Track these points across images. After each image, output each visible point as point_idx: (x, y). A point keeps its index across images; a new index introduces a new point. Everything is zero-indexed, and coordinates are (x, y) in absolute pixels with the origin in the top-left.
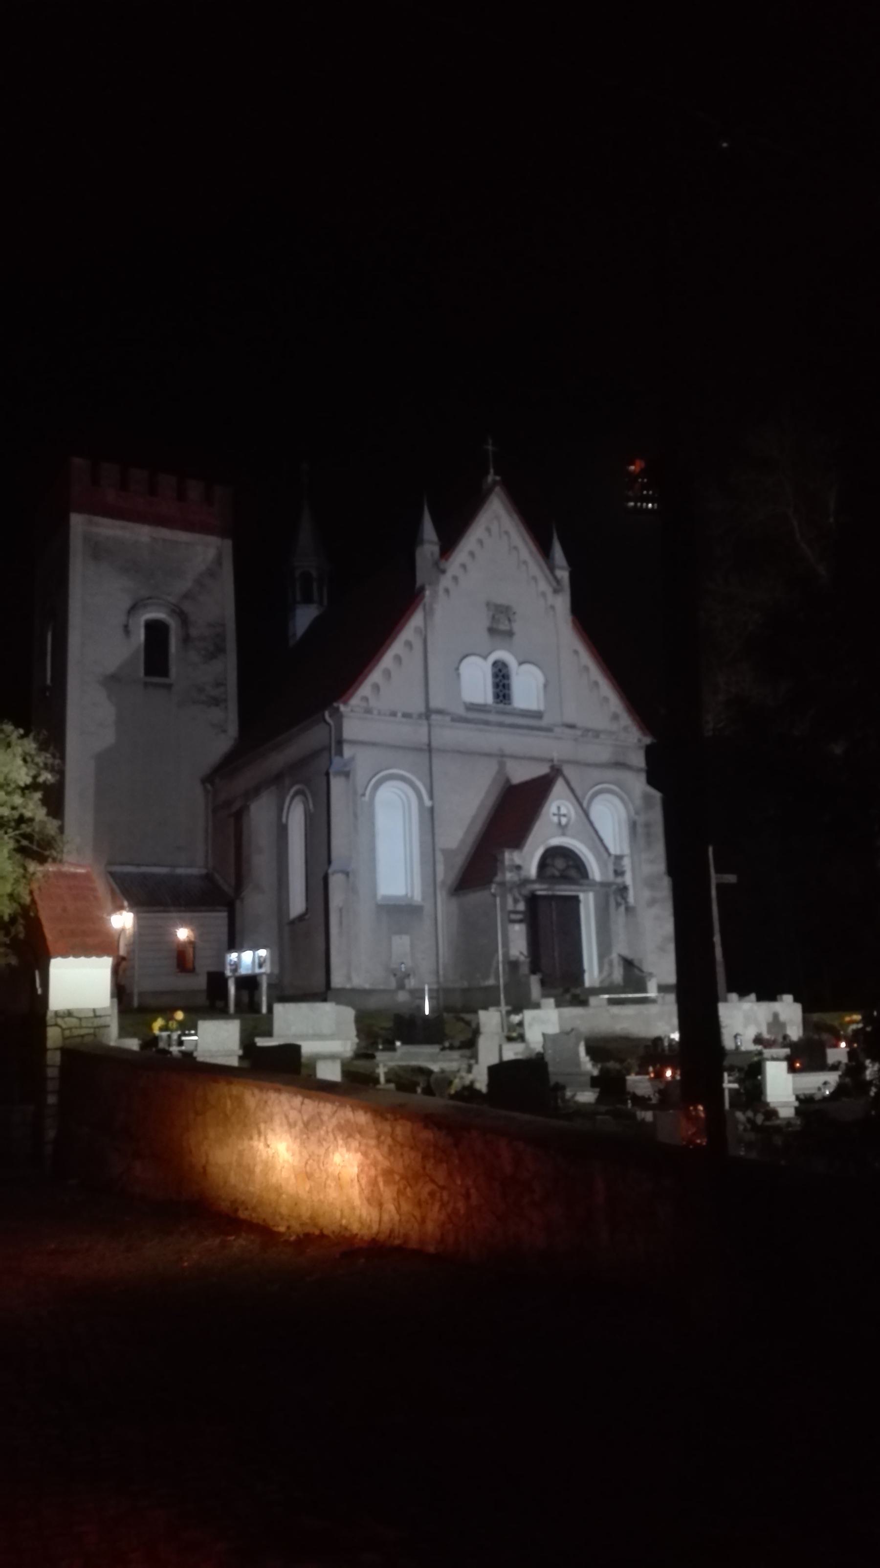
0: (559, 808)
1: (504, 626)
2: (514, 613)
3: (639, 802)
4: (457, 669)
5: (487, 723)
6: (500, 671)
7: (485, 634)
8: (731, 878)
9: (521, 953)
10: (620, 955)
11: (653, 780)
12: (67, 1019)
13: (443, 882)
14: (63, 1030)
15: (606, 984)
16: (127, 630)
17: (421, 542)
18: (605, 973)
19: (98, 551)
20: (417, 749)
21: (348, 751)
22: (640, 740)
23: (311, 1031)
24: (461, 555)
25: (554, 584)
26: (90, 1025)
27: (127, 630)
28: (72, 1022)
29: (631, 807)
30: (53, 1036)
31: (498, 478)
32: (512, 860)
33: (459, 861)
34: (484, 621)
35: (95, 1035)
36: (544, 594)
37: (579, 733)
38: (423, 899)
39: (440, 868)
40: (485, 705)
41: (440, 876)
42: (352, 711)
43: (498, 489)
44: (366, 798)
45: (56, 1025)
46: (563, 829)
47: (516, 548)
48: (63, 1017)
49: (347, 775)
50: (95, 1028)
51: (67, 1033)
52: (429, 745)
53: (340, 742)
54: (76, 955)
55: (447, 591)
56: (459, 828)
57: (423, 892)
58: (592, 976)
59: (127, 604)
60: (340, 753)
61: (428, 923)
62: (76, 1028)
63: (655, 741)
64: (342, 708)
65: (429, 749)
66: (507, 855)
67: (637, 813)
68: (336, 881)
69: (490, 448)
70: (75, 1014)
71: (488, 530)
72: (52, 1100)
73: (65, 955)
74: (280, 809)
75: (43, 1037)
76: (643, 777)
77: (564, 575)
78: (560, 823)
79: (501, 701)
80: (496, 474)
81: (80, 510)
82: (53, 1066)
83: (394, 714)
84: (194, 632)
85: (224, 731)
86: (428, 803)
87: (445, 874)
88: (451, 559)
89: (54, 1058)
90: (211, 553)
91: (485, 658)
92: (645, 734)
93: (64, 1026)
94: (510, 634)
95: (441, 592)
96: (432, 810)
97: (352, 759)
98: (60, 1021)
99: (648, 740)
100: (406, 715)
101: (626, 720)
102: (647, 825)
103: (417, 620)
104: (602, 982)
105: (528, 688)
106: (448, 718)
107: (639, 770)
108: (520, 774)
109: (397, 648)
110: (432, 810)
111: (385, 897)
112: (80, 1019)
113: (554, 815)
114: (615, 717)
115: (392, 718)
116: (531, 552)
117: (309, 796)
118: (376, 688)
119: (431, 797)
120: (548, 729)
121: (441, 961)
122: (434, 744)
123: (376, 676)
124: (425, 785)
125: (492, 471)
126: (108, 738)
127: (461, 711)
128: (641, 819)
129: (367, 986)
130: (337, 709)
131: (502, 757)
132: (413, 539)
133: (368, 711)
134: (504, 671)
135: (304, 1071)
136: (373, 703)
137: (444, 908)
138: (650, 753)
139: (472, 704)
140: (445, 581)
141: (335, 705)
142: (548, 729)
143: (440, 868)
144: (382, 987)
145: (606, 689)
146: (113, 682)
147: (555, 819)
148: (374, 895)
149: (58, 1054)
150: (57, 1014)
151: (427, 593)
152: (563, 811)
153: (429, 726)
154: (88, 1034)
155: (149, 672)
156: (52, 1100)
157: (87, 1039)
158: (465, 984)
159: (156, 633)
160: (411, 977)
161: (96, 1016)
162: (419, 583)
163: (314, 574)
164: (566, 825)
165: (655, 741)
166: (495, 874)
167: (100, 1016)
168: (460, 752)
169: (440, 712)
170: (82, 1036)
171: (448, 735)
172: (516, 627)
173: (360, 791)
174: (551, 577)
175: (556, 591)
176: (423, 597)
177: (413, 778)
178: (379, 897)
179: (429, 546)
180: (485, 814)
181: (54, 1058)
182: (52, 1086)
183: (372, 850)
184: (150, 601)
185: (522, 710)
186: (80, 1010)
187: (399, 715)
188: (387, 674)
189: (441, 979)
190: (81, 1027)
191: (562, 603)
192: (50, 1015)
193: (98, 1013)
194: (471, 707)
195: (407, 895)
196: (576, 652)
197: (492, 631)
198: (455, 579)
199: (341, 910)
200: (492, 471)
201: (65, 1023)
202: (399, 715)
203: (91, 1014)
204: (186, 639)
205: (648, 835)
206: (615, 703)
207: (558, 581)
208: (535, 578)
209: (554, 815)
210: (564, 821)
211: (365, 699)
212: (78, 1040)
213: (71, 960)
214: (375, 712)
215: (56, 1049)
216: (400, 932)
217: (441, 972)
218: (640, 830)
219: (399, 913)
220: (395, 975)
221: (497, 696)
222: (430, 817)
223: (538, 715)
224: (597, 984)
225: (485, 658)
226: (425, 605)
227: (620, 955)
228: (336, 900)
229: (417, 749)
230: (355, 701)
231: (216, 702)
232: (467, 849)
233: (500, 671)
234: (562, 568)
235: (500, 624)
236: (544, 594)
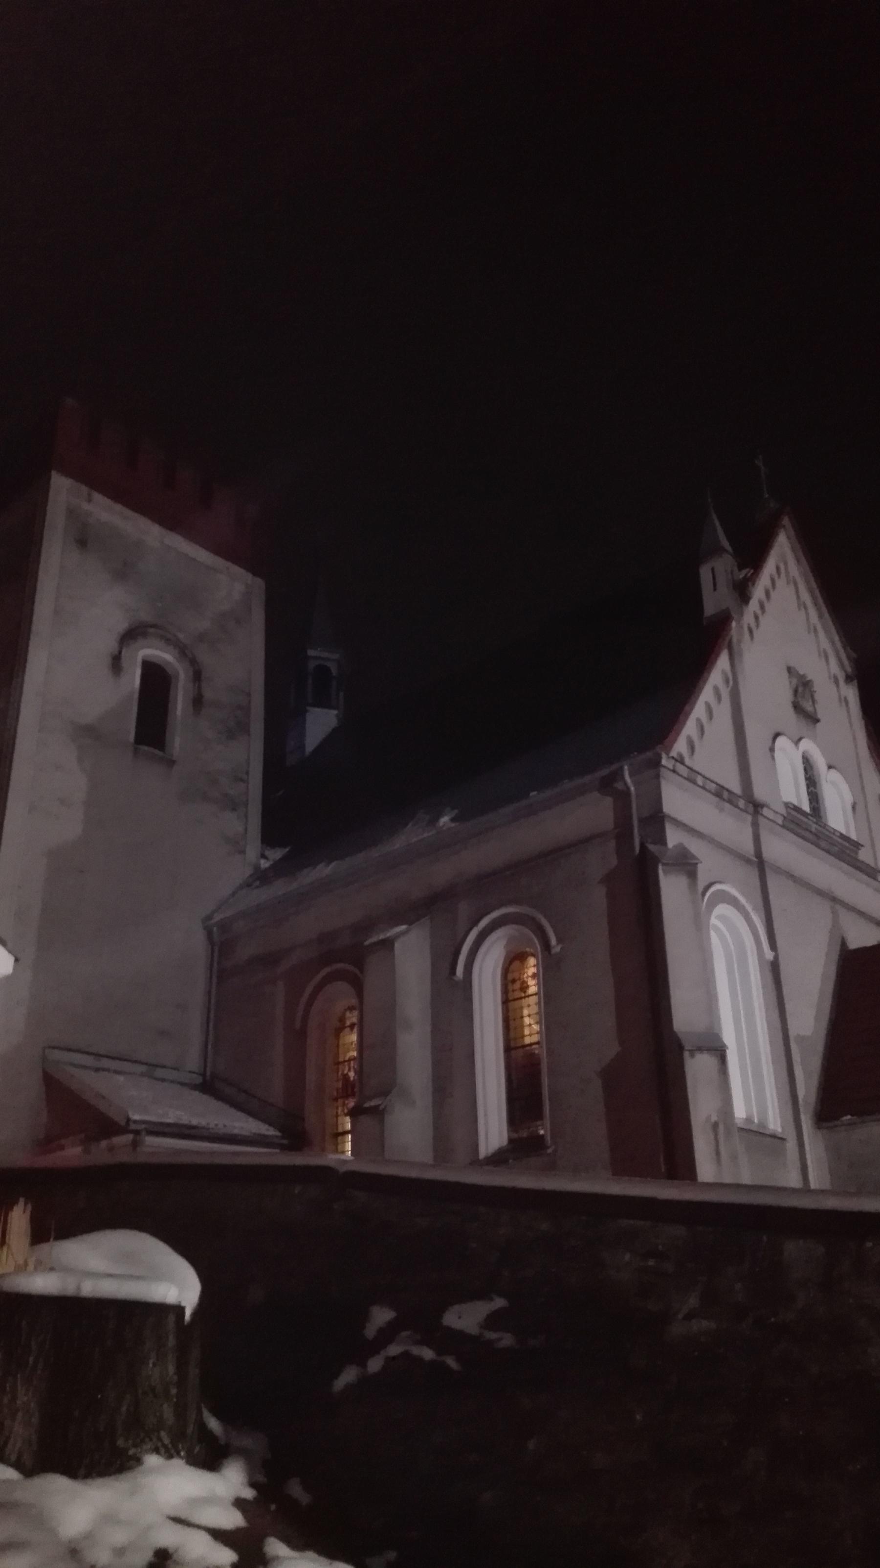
4: (772, 750)
16: (116, 663)
19: (83, 538)
27: (116, 663)
41: (801, 1093)
52: (758, 854)
59: (122, 626)
65: (760, 864)
81: (67, 472)
84: (208, 694)
85: (242, 852)
86: (769, 955)
90: (238, 589)
103: (723, 662)
119: (773, 946)
122: (766, 854)
126: (69, 827)
140: (748, 618)
146: (89, 735)
151: (734, 624)
155: (140, 739)
159: (156, 682)
163: (334, 672)
177: (749, 908)
184: (152, 630)
199: (715, 1126)
204: (198, 702)
226: (730, 642)
231: (233, 804)
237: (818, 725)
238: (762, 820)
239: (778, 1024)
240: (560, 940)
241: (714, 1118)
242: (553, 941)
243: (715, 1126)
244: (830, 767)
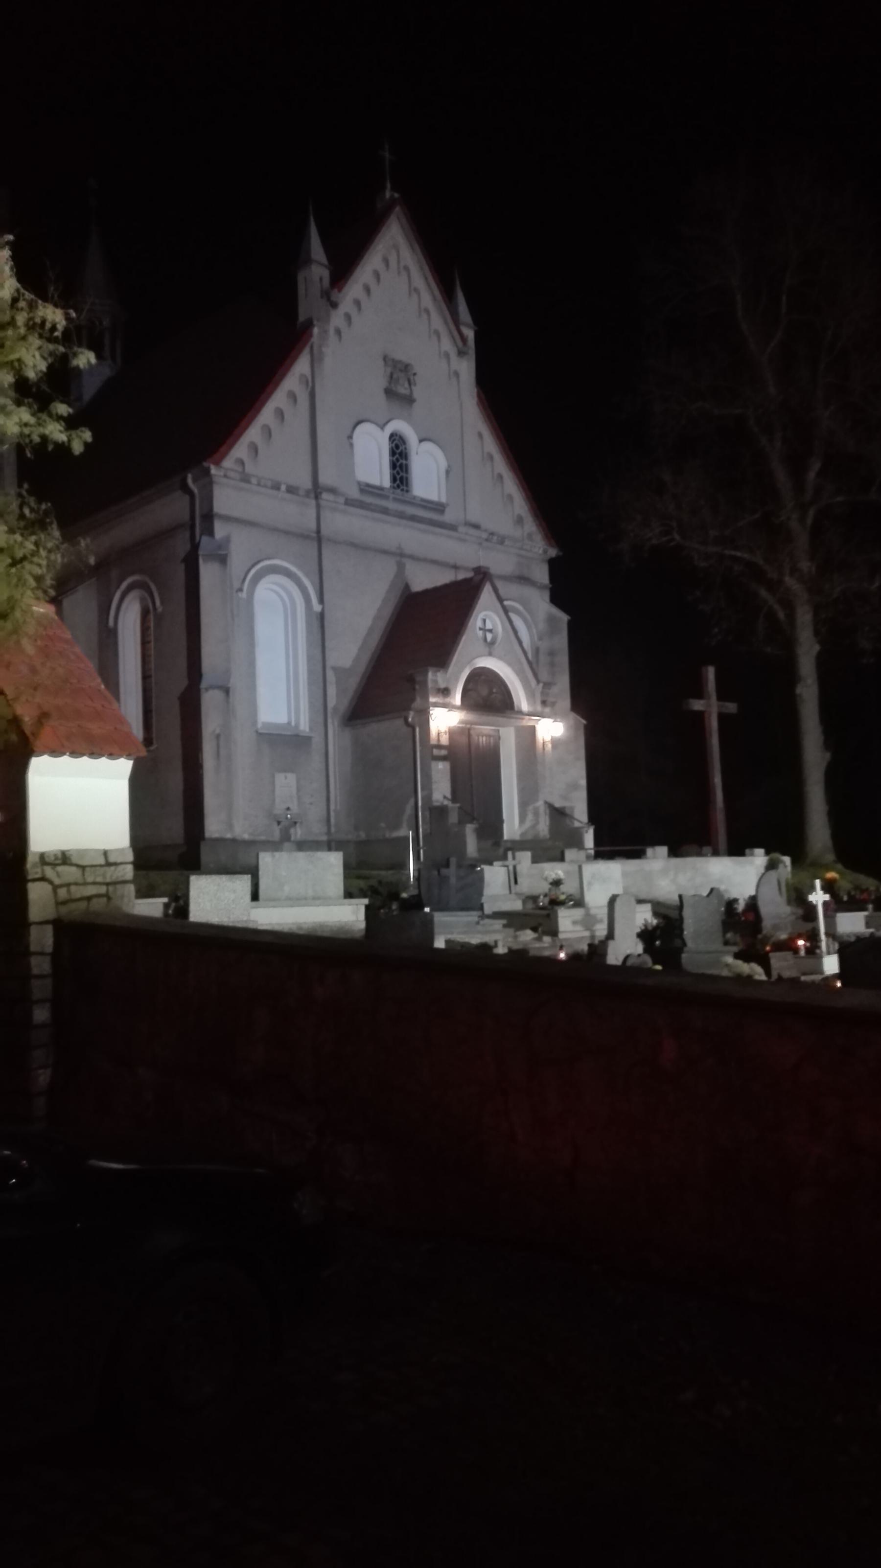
0: (484, 621)
1: (403, 390)
2: (415, 374)
3: (542, 626)
4: (350, 437)
5: (385, 511)
6: (397, 447)
7: (382, 396)
8: (732, 707)
9: (445, 797)
10: (546, 803)
11: (557, 598)
12: (60, 869)
13: (335, 709)
14: (55, 888)
15: (529, 837)
17: (308, 261)
18: (528, 823)
20: (304, 537)
21: (220, 530)
22: (545, 552)
23: (310, 893)
24: (354, 289)
25: (460, 344)
26: (99, 879)
28: (69, 873)
29: (534, 631)
30: (39, 899)
31: (396, 195)
32: (436, 682)
33: (353, 683)
34: (378, 381)
35: (107, 896)
36: (447, 356)
37: (484, 535)
38: (311, 729)
39: (332, 691)
40: (381, 488)
41: (332, 702)
42: (225, 476)
43: (398, 209)
44: (244, 595)
45: (43, 879)
46: (490, 647)
47: (416, 290)
48: (53, 865)
49: (223, 560)
50: (107, 884)
51: (62, 893)
52: (318, 531)
53: (209, 517)
54: (75, 753)
55: (338, 332)
56: (355, 638)
57: (311, 721)
58: (512, 826)
60: (211, 533)
61: (317, 761)
62: (76, 884)
63: (561, 554)
64: (213, 470)
65: (319, 538)
66: (430, 675)
67: (540, 639)
68: (210, 700)
69: (387, 155)
70: (75, 860)
71: (386, 261)
72: (41, 1015)
73: (55, 752)
74: (104, 610)
75: (22, 901)
76: (546, 595)
77: (470, 333)
78: (485, 639)
79: (398, 486)
80: (393, 189)
82: (42, 954)
83: (276, 487)
86: (317, 608)
87: (338, 699)
88: (346, 289)
89: (42, 939)
91: (382, 427)
92: (551, 545)
93: (57, 881)
94: (409, 400)
95: (332, 331)
96: (322, 616)
97: (227, 540)
98: (49, 872)
99: (553, 552)
100: (291, 490)
101: (531, 526)
102: (552, 653)
103: (302, 365)
104: (522, 835)
105: (428, 473)
106: (342, 500)
107: (541, 587)
108: (423, 580)
109: (278, 399)
110: (322, 616)
111: (266, 725)
112: (83, 868)
113: (480, 629)
114: (519, 521)
115: (275, 492)
116: (435, 299)
117: (153, 587)
118: (254, 449)
119: (321, 601)
120: (453, 528)
121: (332, 807)
122: (324, 531)
123: (253, 433)
124: (313, 583)
125: (389, 185)
127: (355, 493)
128: (544, 645)
129: (246, 836)
130: (207, 472)
131: (400, 556)
132: (297, 258)
133: (246, 478)
134: (402, 448)
135: (837, 946)
136: (249, 468)
137: (338, 740)
138: (553, 565)
139: (368, 485)
140: (337, 319)
141: (205, 464)
142: (453, 528)
143: (332, 691)
144: (263, 838)
145: (511, 486)
147: (480, 633)
148: (255, 722)
149: (49, 929)
150: (43, 859)
151: (316, 330)
152: (489, 626)
153: (318, 507)
154: (98, 896)
156: (41, 1015)
157: (98, 905)
158: (363, 835)
160: (298, 825)
161: (109, 864)
162: (302, 318)
164: (493, 643)
165: (561, 554)
166: (413, 700)
167: (115, 864)
168: (354, 545)
169: (333, 491)
170: (89, 899)
171: (341, 522)
172: (418, 392)
173: (236, 585)
174: (456, 333)
175: (461, 353)
176: (311, 335)
177: (300, 574)
178: (259, 725)
179: (318, 271)
180: (382, 624)
181: (42, 939)
182: (41, 989)
183: (251, 664)
185: (423, 500)
186: (83, 853)
187: (283, 488)
188: (268, 432)
189: (333, 830)
190: (85, 884)
191: (467, 368)
192: (31, 859)
193: (112, 859)
194: (367, 489)
195: (289, 723)
196: (480, 435)
197: (389, 393)
198: (348, 317)
199: (218, 737)
200: (389, 185)
201: (58, 875)
202: (283, 488)
203: (102, 861)
205: (552, 665)
206: (520, 505)
207: (464, 340)
208: (437, 334)
209: (480, 629)
210: (489, 636)
211: (241, 462)
212: (83, 905)
213: (66, 760)
214: (254, 481)
215: (46, 922)
216: (286, 769)
217: (333, 820)
218: (543, 659)
219: (284, 745)
220: (279, 823)
221: (394, 479)
222: (320, 624)
223: (439, 508)
224: (517, 837)
225: (382, 427)
226: (312, 348)
227: (546, 803)
228: (210, 724)
229: (304, 537)
230: (228, 463)
232: (361, 668)
233: (397, 447)
234: (467, 325)
235: (399, 385)
236: (447, 356)
237: (415, 405)
238: (323, 503)
239: (319, 657)
240: (162, 603)
241: (218, 731)
242: (158, 603)
243: (218, 737)
244: (421, 441)
